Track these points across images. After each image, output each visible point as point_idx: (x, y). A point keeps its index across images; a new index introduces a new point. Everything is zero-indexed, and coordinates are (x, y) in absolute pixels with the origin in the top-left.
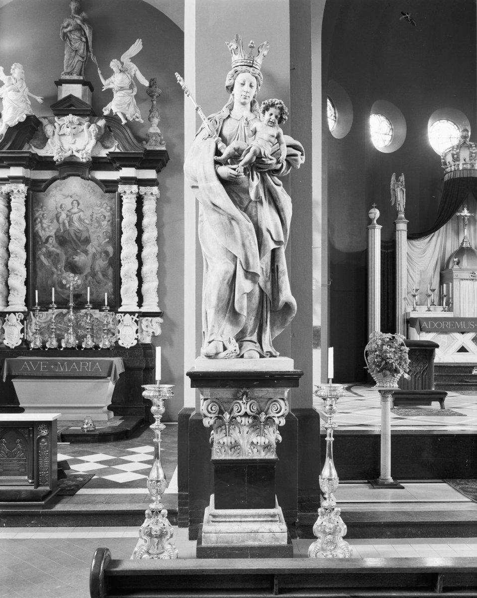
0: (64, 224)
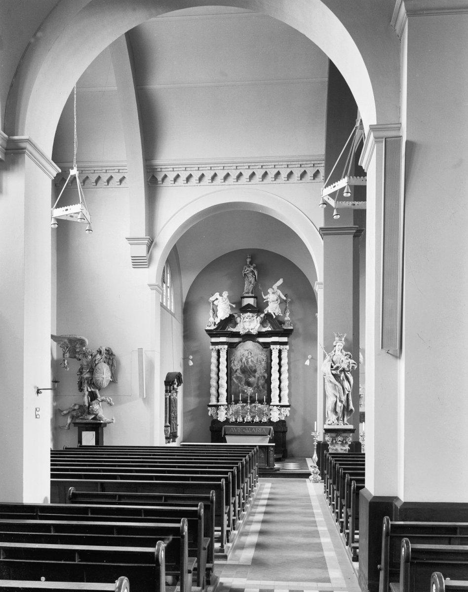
0: (244, 363)
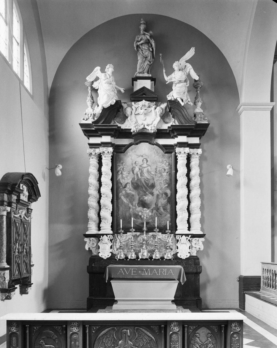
0: (137, 175)
